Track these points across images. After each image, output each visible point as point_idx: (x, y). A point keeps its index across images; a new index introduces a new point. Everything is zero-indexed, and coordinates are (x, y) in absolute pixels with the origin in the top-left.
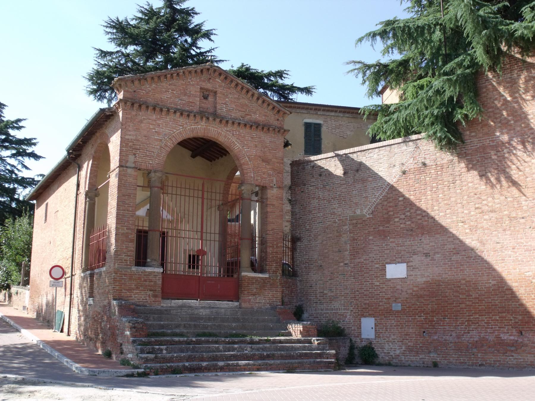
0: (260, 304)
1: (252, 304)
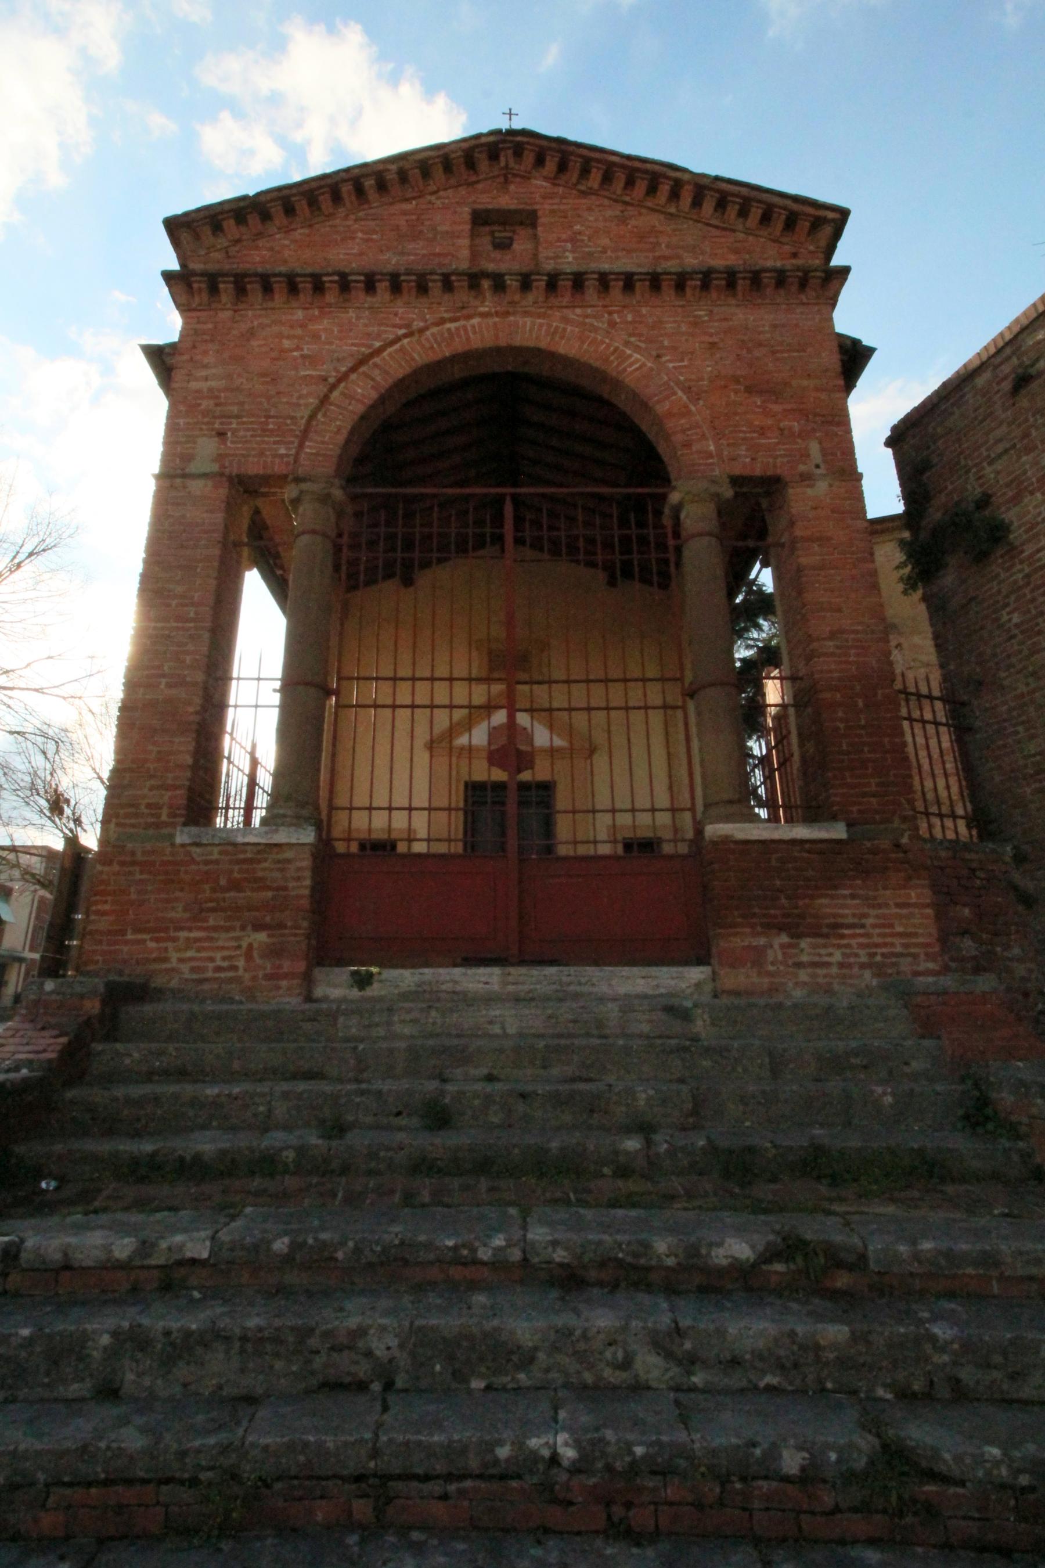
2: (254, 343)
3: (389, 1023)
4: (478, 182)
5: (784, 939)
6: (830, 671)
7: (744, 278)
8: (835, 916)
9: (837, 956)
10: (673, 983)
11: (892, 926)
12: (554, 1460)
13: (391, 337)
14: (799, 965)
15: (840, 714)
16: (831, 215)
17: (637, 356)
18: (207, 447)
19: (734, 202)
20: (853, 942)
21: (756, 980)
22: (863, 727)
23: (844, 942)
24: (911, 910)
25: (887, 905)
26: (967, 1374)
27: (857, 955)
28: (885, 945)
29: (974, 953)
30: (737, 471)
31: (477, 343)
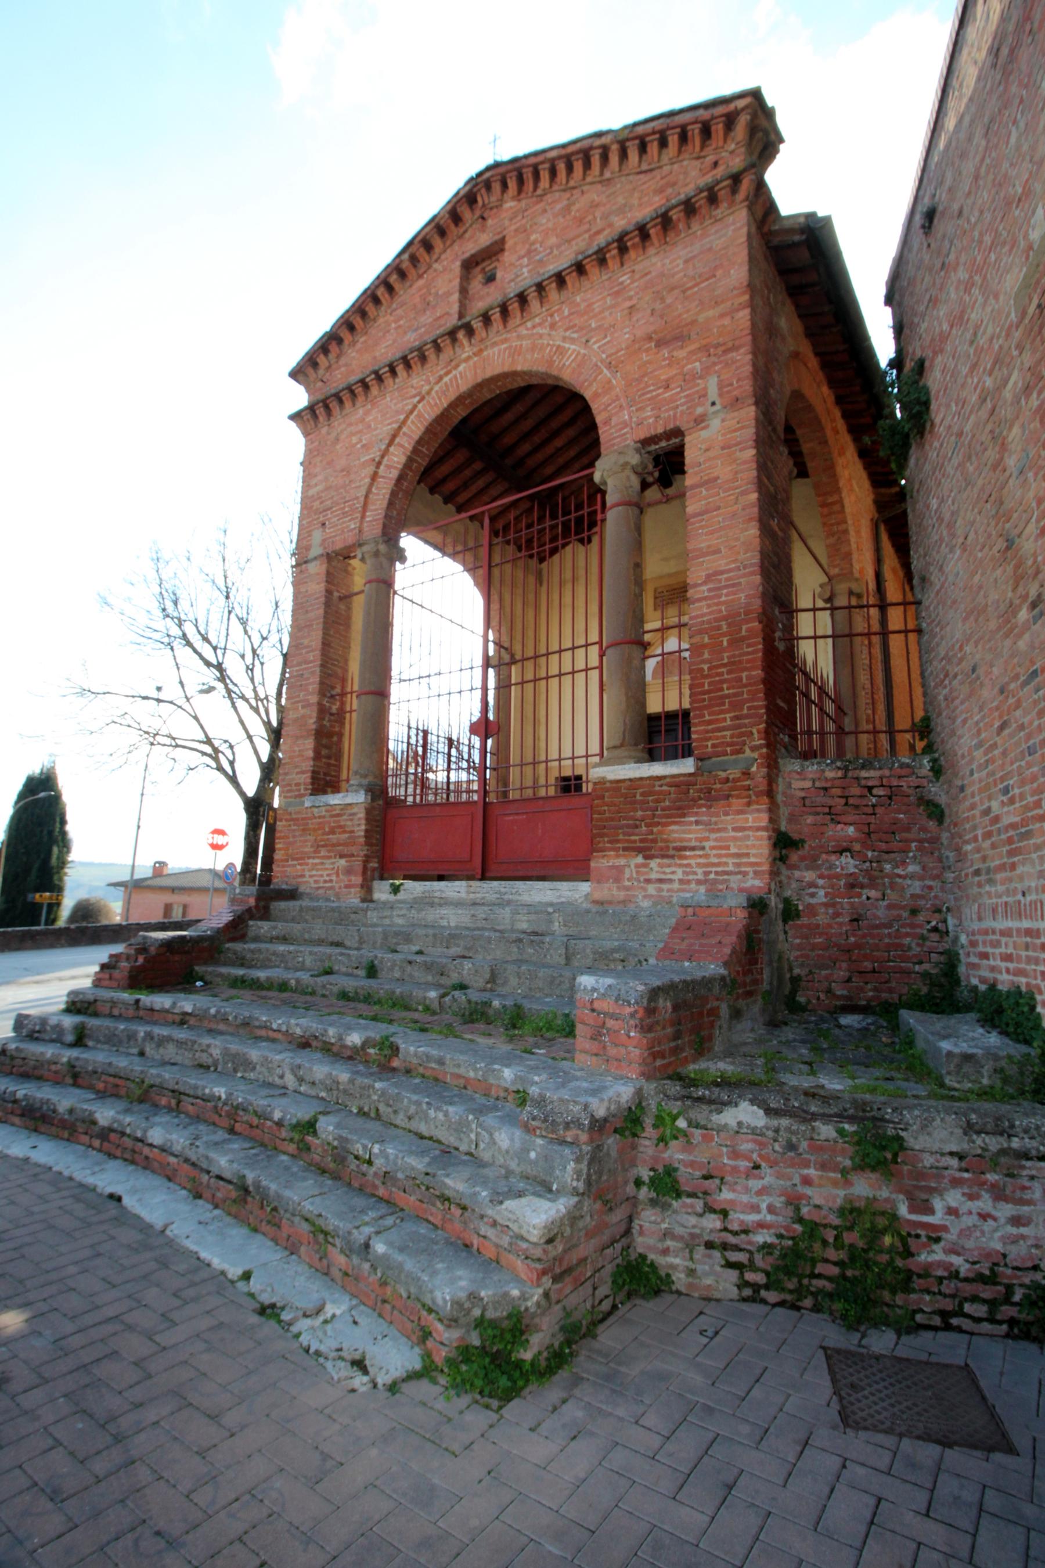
0: (665, 886)
1: (628, 889)
2: (338, 447)
3: (391, 917)
4: (465, 232)
5: (640, 859)
6: (703, 615)
7: (655, 226)
8: (681, 840)
9: (679, 874)
10: (569, 894)
11: (728, 848)
12: (220, 1098)
13: (410, 407)
14: (648, 881)
15: (706, 656)
16: (741, 103)
17: (573, 347)
18: (317, 536)
19: (652, 141)
20: (692, 862)
21: (615, 892)
22: (724, 665)
23: (685, 862)
24: (747, 833)
25: (725, 830)
26: (382, 1108)
27: (695, 873)
28: (718, 865)
29: (852, 870)
30: (643, 434)
31: (464, 387)
